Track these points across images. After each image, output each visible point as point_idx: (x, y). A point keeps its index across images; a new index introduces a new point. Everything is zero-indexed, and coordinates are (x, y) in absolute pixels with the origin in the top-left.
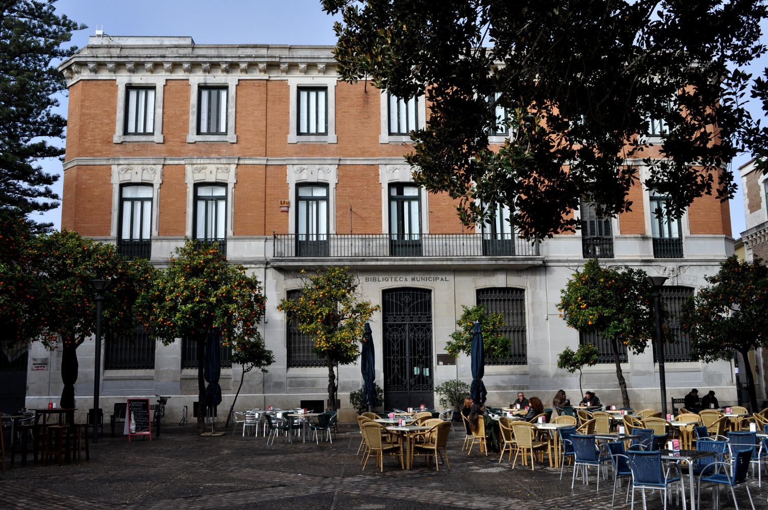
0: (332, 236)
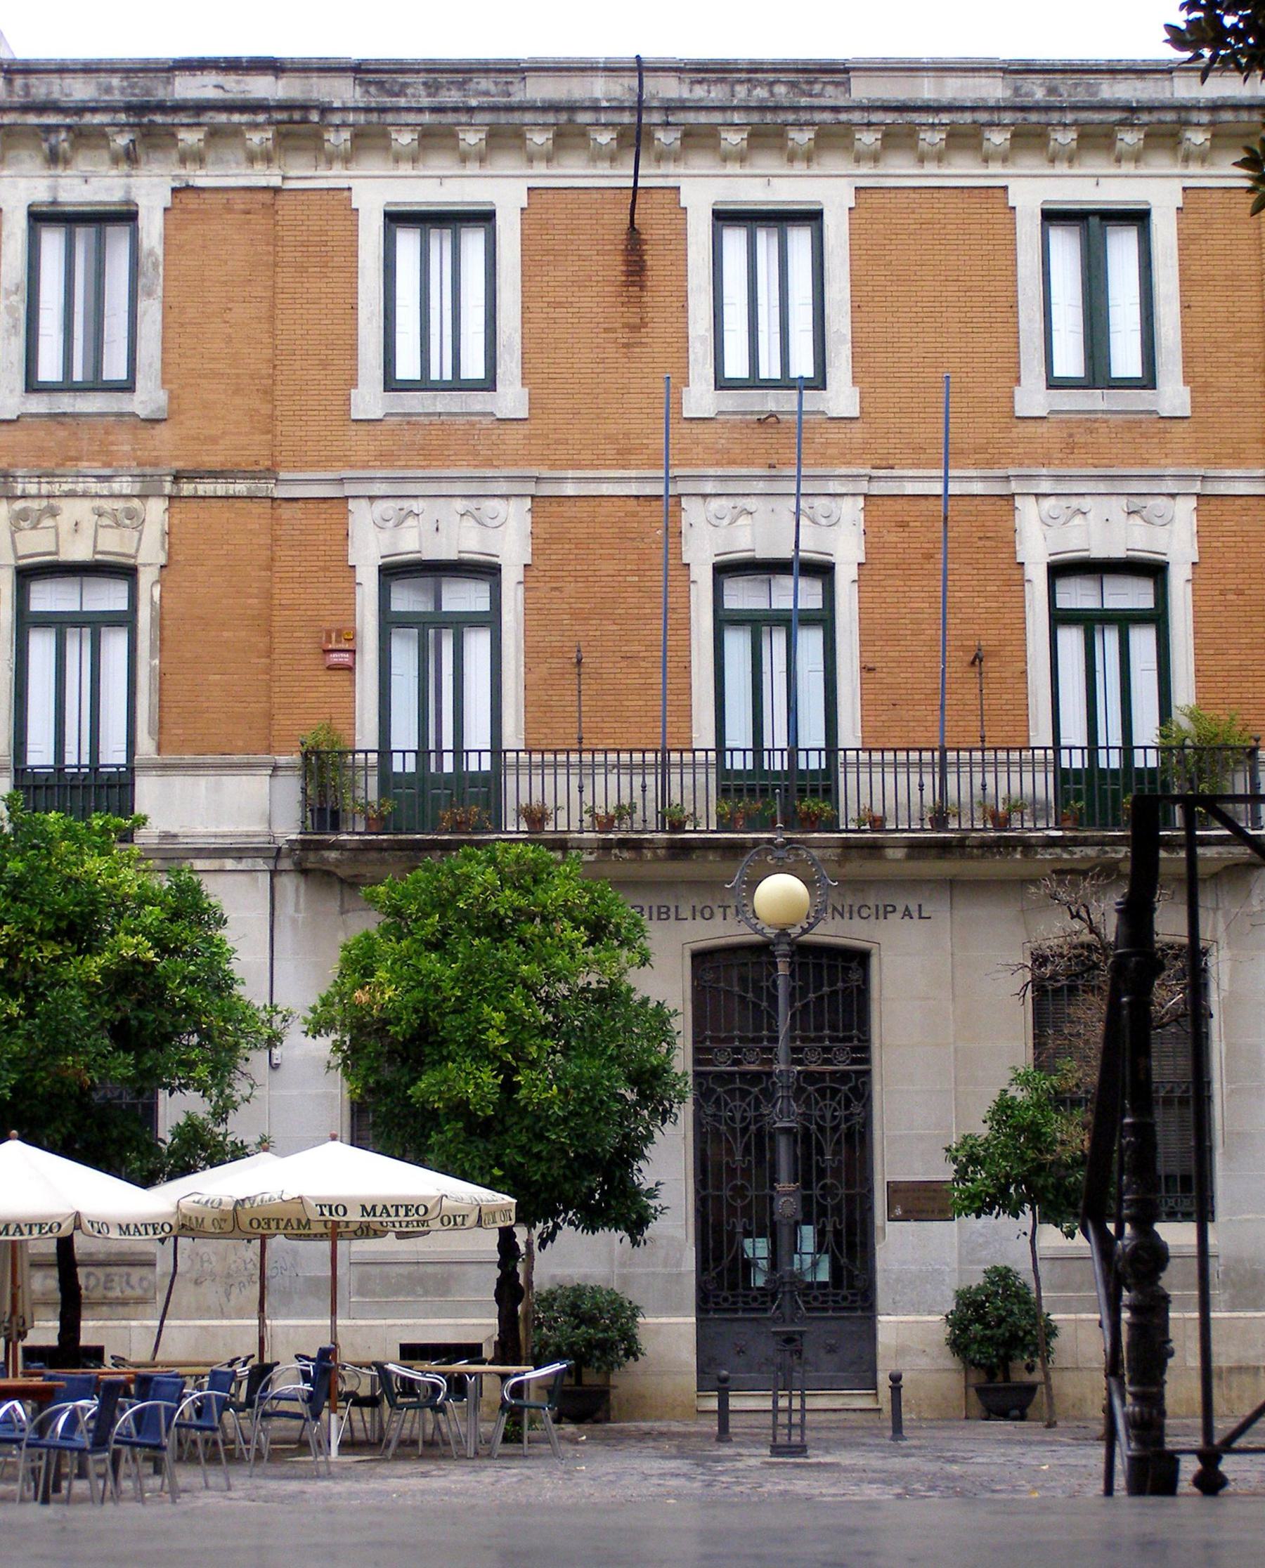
0: (511, 756)
